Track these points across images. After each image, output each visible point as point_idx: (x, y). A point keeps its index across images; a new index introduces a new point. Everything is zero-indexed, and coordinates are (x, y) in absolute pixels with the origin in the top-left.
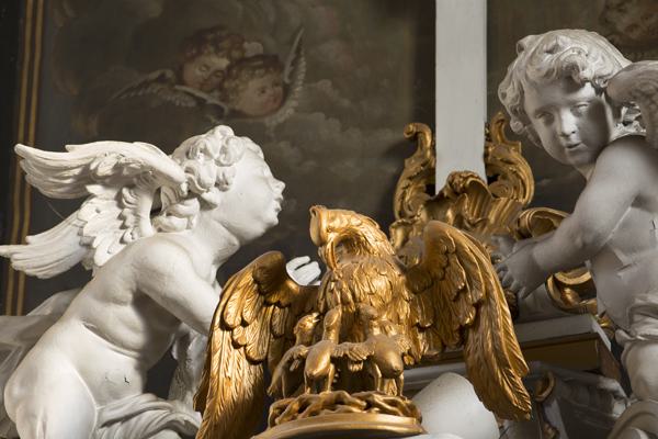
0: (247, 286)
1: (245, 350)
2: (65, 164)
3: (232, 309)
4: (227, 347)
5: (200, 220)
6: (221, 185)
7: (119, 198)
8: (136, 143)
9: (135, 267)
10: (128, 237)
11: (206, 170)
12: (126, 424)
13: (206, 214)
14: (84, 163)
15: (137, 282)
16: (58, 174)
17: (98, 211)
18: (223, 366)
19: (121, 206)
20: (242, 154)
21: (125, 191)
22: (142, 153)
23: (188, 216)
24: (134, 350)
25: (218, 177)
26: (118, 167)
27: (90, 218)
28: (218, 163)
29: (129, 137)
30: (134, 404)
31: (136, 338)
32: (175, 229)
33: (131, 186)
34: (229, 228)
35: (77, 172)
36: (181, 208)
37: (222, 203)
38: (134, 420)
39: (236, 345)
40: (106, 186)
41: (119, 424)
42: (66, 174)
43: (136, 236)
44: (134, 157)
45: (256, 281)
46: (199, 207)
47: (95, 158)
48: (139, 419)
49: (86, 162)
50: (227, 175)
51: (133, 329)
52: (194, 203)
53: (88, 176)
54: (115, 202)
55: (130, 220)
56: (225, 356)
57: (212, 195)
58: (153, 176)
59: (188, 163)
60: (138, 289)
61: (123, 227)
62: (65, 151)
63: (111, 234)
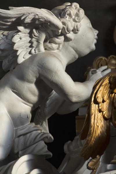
0: (106, 84)
1: (103, 113)
2: (9, 16)
3: (99, 95)
4: (97, 111)
5: (63, 46)
6: (75, 31)
7: (31, 34)
8: (42, 9)
9: (39, 67)
10: (33, 51)
11: (71, 25)
12: (25, 136)
13: (66, 43)
14: (18, 16)
15: (40, 74)
16: (5, 20)
17: (20, 38)
18: (96, 121)
19: (31, 37)
20: (84, 17)
21: (34, 30)
22: (44, 14)
23: (59, 44)
24: (32, 103)
25: (74, 28)
26: (34, 20)
27: (18, 41)
28: (74, 20)
29: (39, 6)
30: (29, 128)
31: (34, 98)
32: (53, 49)
33: (37, 29)
34: (76, 51)
35: (14, 20)
36: (57, 40)
37: (74, 39)
38: (28, 135)
39: (100, 111)
40: (26, 27)
41: (22, 136)
42: (9, 20)
43: (37, 51)
44: (42, 16)
45: (110, 83)
46: (64, 39)
47: (24, 14)
48: (31, 135)
49: (19, 16)
50: (78, 27)
51: (34, 94)
52: (62, 38)
53: (19, 21)
54: (29, 35)
55: (35, 44)
56: (96, 116)
57: (70, 35)
58: (50, 26)
59: (63, 20)
60: (39, 77)
61: (31, 46)
62: (9, 9)
63: (25, 49)
